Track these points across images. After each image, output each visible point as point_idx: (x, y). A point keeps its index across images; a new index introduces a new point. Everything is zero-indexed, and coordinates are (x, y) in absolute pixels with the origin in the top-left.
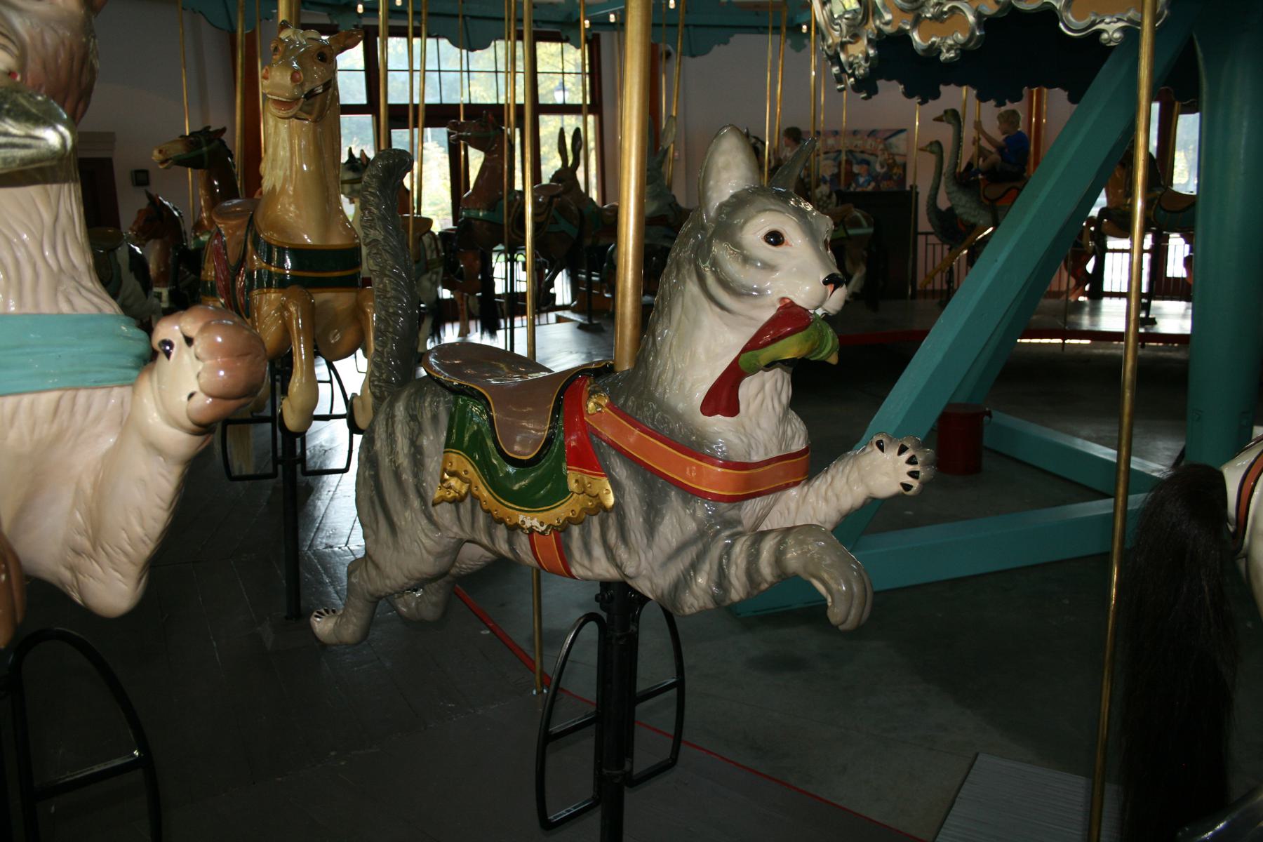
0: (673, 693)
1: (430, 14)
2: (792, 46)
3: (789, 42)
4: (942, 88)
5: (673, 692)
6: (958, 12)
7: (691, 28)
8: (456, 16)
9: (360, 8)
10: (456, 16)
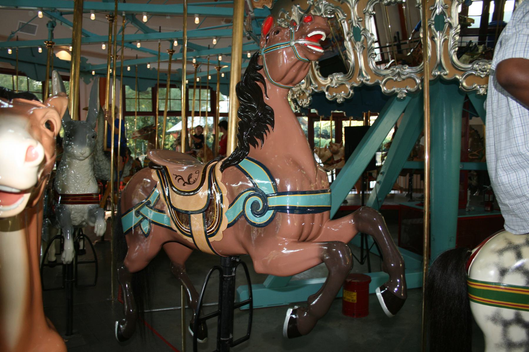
1: (157, 80)
8: (135, 78)
9: (93, 73)
10: (135, 78)
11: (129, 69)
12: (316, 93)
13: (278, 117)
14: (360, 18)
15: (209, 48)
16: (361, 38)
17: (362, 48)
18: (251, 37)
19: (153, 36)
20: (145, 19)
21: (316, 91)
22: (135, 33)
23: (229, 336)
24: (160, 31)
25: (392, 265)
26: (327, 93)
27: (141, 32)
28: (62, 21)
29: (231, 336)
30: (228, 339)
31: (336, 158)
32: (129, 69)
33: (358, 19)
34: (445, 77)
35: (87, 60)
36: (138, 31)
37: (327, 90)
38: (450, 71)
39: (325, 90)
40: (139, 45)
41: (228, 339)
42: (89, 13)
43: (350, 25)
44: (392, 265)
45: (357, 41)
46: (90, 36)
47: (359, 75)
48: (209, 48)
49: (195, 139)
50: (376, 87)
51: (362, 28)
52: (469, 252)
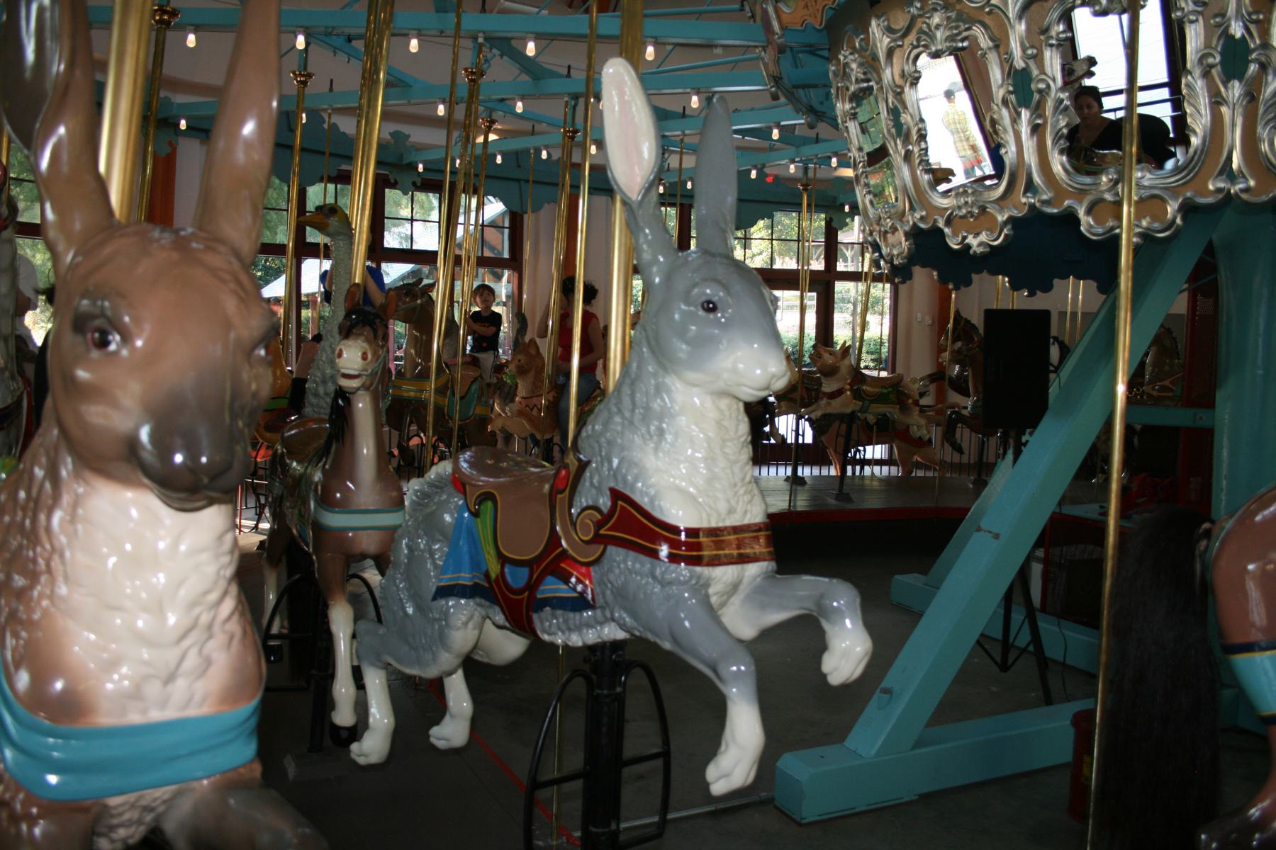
0: (659, 763)
4: (1056, 282)
5: (659, 763)
7: (522, 182)
11: (499, 160)
12: (922, 230)
13: (973, 283)
14: (1257, 12)
15: (684, 115)
16: (1246, 68)
17: (1248, 98)
18: (780, 94)
19: (554, 85)
20: (531, 49)
21: (922, 226)
22: (514, 79)
23: (609, 825)
24: (569, 75)
25: (338, 495)
26: (947, 230)
27: (525, 78)
28: (349, 55)
30: (607, 830)
31: (829, 386)
32: (499, 160)
33: (1250, 14)
34: (1244, 196)
35: (409, 136)
36: (520, 74)
37: (948, 222)
38: (1258, 182)
39: (941, 224)
40: (519, 107)
41: (607, 830)
42: (407, 36)
43: (1007, 61)
44: (338, 495)
45: (1233, 77)
46: (411, 86)
47: (1220, 173)
48: (684, 115)
49: (477, 327)
50: (1070, 219)
51: (1035, 72)
52: (687, 536)
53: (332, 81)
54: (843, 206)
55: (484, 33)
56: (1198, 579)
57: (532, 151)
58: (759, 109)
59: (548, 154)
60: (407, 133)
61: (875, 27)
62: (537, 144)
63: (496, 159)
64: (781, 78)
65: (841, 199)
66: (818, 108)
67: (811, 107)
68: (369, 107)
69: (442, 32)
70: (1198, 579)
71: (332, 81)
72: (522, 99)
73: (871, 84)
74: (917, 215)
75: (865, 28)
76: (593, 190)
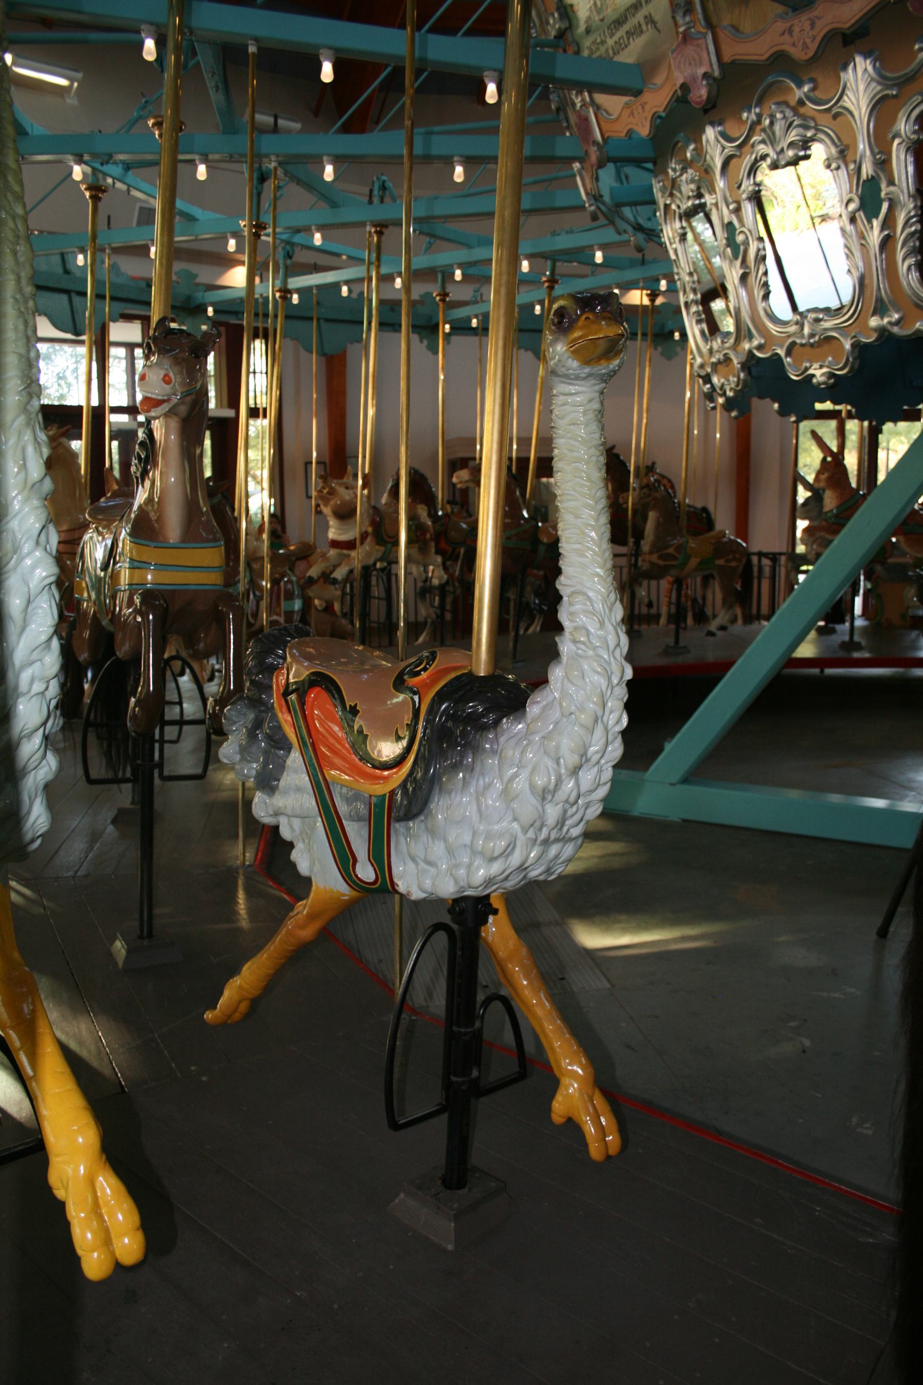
2: (662, 354)
3: (425, 342)
6: (835, 341)
7: (73, 295)
29: (475, 1073)
39: (781, 352)
53: (109, 217)
54: (672, 333)
55: (277, 156)
56: (630, 524)
57: (314, 291)
58: (579, 232)
59: (350, 291)
60: (195, 272)
61: (710, 133)
62: (448, 262)
63: (340, 290)
64: (601, 196)
65: (670, 325)
66: (647, 225)
67: (639, 224)
68: (302, 738)
69: (231, 157)
70: (630, 524)
71: (109, 217)
72: (321, 228)
73: (703, 201)
74: (756, 343)
75: (697, 139)
76: (382, 325)
